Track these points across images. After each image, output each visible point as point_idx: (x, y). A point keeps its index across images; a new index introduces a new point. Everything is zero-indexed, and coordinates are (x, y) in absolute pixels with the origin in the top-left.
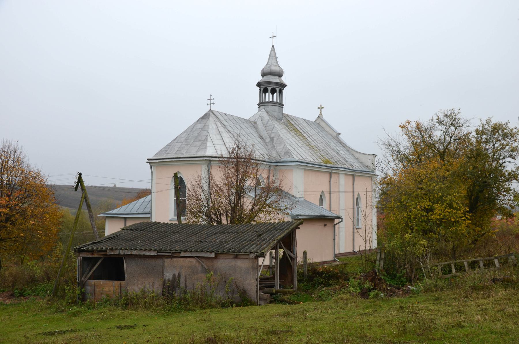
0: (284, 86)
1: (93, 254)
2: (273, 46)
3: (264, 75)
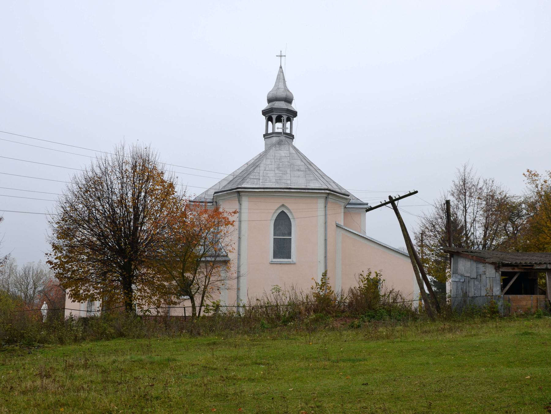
0: (295, 114)
1: (514, 269)
2: (281, 67)
3: (270, 101)
